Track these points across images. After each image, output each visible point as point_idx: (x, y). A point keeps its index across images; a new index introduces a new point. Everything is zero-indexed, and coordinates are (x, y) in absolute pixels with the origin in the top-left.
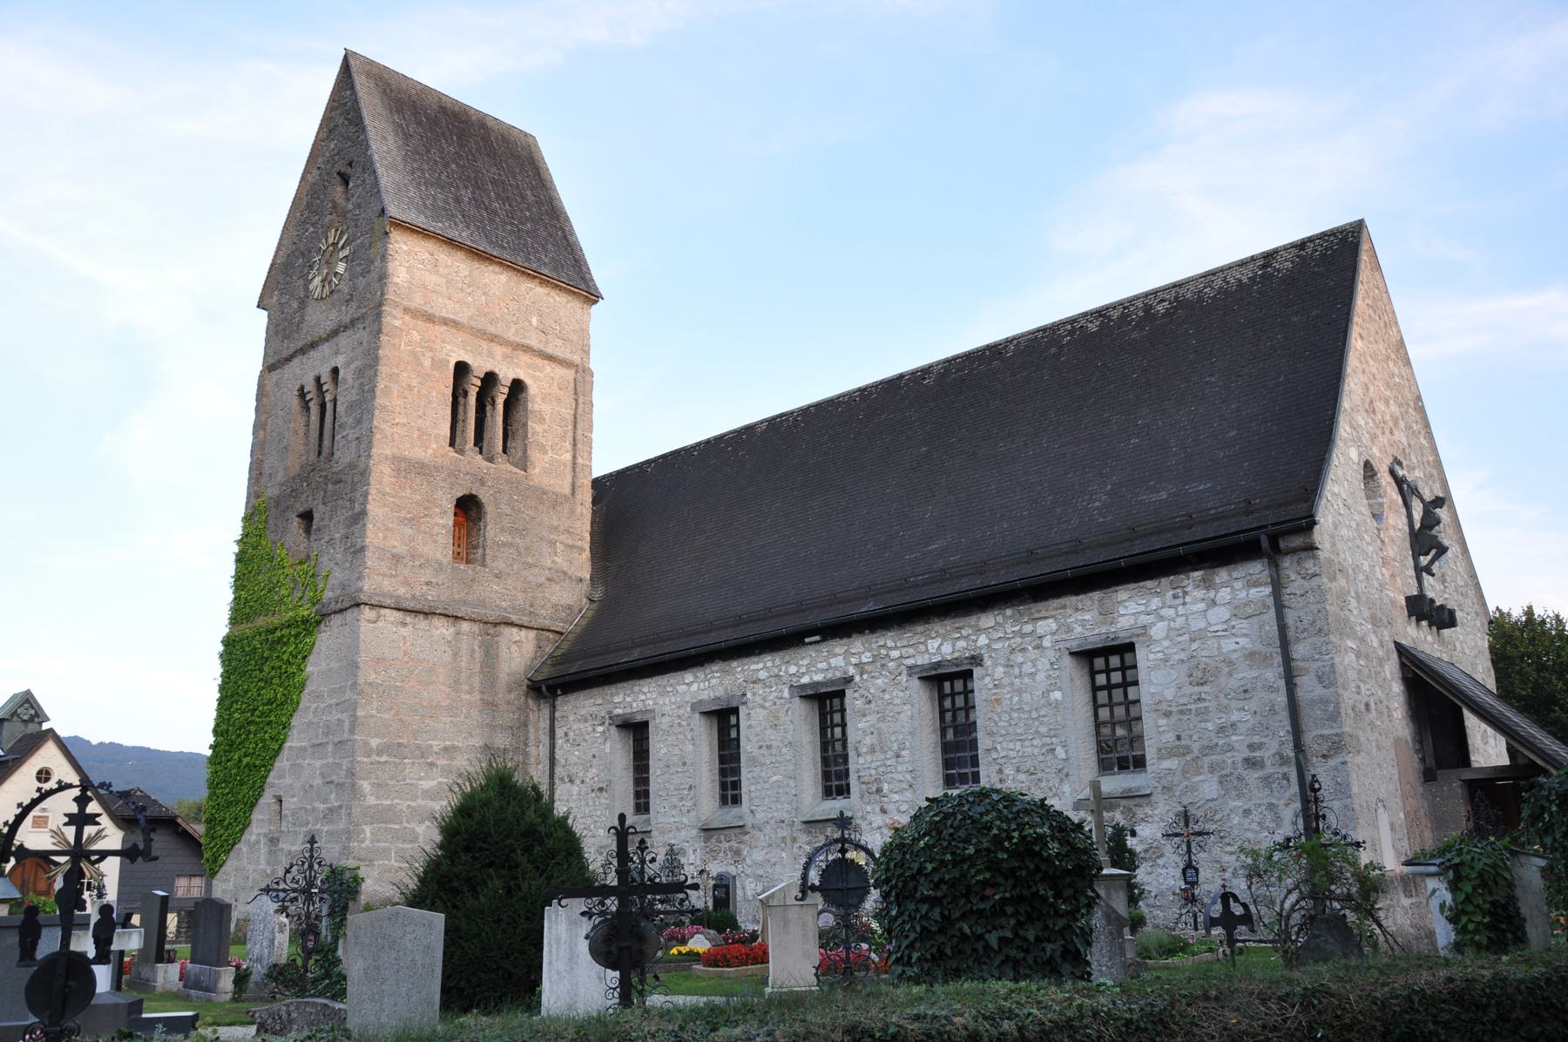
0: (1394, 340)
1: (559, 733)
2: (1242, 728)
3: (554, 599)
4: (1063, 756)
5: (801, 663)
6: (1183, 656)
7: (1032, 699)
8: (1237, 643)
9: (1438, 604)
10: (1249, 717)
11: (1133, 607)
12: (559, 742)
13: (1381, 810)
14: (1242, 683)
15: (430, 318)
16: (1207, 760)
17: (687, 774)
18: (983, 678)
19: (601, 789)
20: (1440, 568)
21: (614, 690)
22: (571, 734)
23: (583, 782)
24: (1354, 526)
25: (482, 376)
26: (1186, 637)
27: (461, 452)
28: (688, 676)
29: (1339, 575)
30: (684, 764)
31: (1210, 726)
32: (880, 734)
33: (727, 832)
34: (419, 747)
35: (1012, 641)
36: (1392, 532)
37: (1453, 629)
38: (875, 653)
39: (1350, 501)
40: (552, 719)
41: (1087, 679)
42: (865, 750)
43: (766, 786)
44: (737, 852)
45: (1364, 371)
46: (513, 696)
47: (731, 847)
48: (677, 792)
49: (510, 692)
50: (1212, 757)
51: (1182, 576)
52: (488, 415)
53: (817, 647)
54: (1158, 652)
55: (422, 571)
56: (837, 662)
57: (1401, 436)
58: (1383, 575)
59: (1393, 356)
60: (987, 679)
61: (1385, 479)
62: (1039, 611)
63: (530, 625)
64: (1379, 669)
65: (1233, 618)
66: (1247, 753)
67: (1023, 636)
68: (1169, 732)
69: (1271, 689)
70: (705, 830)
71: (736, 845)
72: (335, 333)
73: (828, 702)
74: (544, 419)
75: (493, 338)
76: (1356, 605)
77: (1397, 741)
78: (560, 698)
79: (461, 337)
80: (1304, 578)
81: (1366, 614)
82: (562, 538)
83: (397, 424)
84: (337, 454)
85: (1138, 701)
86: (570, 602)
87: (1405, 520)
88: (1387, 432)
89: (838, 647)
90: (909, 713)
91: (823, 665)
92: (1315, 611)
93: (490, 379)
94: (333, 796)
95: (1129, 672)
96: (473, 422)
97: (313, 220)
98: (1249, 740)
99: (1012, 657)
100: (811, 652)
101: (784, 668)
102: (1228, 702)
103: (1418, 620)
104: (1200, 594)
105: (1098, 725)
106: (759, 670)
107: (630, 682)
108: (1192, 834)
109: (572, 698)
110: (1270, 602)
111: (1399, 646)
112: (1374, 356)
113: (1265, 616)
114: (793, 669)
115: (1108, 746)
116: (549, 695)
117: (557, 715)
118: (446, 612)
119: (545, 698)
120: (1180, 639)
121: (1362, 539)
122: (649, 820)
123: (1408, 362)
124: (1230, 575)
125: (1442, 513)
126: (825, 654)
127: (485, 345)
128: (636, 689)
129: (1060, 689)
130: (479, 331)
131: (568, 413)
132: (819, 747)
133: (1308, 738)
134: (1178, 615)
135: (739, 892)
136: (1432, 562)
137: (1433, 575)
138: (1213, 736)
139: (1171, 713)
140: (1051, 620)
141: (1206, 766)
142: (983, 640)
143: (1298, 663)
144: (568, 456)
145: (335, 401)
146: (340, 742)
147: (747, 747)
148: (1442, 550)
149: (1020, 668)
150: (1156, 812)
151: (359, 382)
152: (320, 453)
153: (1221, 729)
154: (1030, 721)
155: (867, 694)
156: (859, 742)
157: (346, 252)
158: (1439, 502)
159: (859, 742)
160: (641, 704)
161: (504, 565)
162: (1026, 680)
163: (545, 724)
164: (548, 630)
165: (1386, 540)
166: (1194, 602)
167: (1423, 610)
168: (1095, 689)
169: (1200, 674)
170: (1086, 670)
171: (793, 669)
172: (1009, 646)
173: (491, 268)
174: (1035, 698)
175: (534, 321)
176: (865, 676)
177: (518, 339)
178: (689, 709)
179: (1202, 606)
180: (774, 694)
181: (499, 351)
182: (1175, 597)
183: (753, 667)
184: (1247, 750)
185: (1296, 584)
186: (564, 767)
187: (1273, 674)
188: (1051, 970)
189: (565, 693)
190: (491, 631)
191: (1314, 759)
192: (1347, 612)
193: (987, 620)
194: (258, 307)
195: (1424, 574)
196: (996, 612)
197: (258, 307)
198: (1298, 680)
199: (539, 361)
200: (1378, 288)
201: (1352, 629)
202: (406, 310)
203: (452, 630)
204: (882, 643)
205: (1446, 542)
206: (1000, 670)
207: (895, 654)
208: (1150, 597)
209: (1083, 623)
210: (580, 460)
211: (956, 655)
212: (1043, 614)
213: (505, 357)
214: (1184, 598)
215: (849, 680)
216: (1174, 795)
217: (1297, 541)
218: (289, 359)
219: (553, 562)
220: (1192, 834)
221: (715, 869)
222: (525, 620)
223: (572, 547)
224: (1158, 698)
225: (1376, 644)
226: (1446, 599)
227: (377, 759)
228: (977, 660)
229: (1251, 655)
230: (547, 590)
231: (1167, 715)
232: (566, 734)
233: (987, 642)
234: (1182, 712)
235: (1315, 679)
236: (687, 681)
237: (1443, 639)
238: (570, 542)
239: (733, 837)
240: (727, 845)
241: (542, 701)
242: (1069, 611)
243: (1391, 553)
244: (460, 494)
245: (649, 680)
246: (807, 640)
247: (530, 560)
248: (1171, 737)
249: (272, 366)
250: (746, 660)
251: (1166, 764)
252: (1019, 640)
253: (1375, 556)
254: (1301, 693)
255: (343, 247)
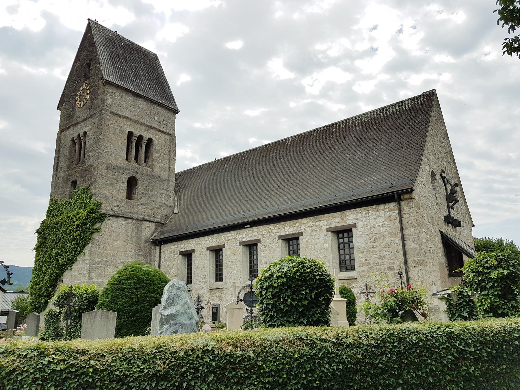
0: (444, 131)
1: (162, 257)
2: (388, 257)
3: (162, 212)
4: (328, 265)
5: (243, 234)
6: (368, 233)
7: (318, 247)
8: (386, 229)
9: (455, 219)
10: (389, 253)
11: (352, 217)
12: (162, 260)
13: (434, 286)
14: (387, 242)
15: (119, 116)
16: (375, 267)
17: (205, 271)
18: (302, 240)
19: (175, 276)
20: (456, 207)
21: (181, 243)
22: (166, 257)
23: (170, 273)
24: (427, 192)
25: (138, 136)
26: (369, 227)
27: (130, 162)
28: (206, 238)
29: (421, 208)
30: (204, 267)
31: (376, 256)
32: (268, 258)
33: (218, 290)
34: (113, 262)
35: (312, 227)
36: (440, 195)
37: (460, 227)
38: (268, 231)
39: (426, 184)
40: (160, 252)
41: (336, 240)
42: (263, 263)
43: (231, 275)
44: (221, 297)
45: (432, 141)
46: (146, 244)
47: (219, 295)
48: (201, 277)
49: (145, 243)
50: (377, 267)
51: (368, 207)
52: (140, 150)
53: (249, 229)
54: (360, 232)
55: (115, 202)
56: (255, 234)
57: (444, 163)
58: (436, 208)
59: (443, 137)
60: (304, 240)
61: (438, 177)
62: (321, 218)
63: (153, 221)
64: (434, 239)
65: (385, 221)
66: (389, 265)
67: (316, 226)
68: (363, 258)
69: (397, 245)
70: (210, 289)
71: (220, 294)
72: (85, 120)
73: (252, 247)
74: (159, 152)
75: (141, 124)
76: (427, 218)
77: (440, 264)
78: (163, 245)
79: (130, 123)
80: (409, 208)
81: (430, 221)
82: (165, 192)
83: (107, 151)
84: (86, 161)
85: (353, 248)
86: (167, 213)
87: (445, 191)
88: (440, 161)
89: (256, 229)
90: (278, 251)
91: (251, 235)
92: (412, 219)
93: (140, 138)
94: (81, 278)
95: (350, 238)
96: (134, 152)
97: (77, 80)
98: (390, 261)
99: (312, 233)
100: (247, 230)
101: (237, 236)
102: (383, 248)
103: (448, 224)
104: (374, 213)
105: (340, 255)
106: (229, 237)
107: (186, 240)
108: (369, 293)
109: (166, 245)
110: (398, 216)
111: (441, 232)
112: (437, 136)
113: (395, 220)
114: (240, 236)
115: (343, 262)
116: (159, 244)
117: (161, 251)
118: (124, 216)
119: (157, 245)
120: (368, 227)
121: (430, 196)
122: (191, 286)
123: (448, 139)
124: (384, 207)
125: (458, 189)
126: (251, 231)
127: (139, 126)
128: (188, 242)
129: (327, 243)
130: (137, 121)
131: (167, 151)
132: (249, 262)
133: (409, 261)
134: (367, 220)
135: (221, 310)
136: (453, 205)
137: (454, 209)
138: (378, 260)
139: (364, 252)
140: (325, 221)
141: (375, 269)
142: (303, 227)
143: (406, 236)
144: (167, 165)
145: (85, 143)
146: (84, 260)
147: (224, 262)
148: (457, 201)
149: (315, 236)
150: (358, 284)
151: (94, 137)
152: (80, 161)
153: (380, 258)
154: (317, 254)
155: (265, 244)
156: (262, 260)
157: (89, 91)
158: (456, 185)
159: (262, 260)
160: (190, 247)
161: (144, 201)
162: (316, 240)
163: (157, 254)
164: (159, 223)
165: (438, 197)
166: (372, 215)
167: (449, 220)
168: (339, 244)
169: (373, 239)
170: (336, 238)
171: (240, 236)
172: (311, 229)
173: (141, 99)
174: (319, 246)
175: (156, 118)
176: (264, 239)
177: (150, 125)
178: (206, 249)
179: (375, 217)
180: (234, 245)
181: (143, 128)
182: (366, 214)
183: (227, 235)
184: (389, 264)
185: (406, 210)
186: (163, 268)
187: (398, 239)
188: (316, 323)
189: (164, 244)
190: (139, 223)
191: (411, 268)
192: (423, 220)
193: (304, 221)
194: (57, 109)
195: (451, 209)
196: (307, 218)
197: (57, 109)
198: (405, 242)
199: (157, 132)
200: (439, 114)
201: (425, 225)
202: (111, 113)
203: (126, 222)
204: (270, 228)
205: (458, 199)
206: (308, 237)
207: (274, 231)
208: (357, 214)
209: (335, 222)
210: (171, 167)
211: (294, 232)
212: (323, 219)
213: (146, 130)
214: (369, 214)
215: (259, 240)
216: (364, 279)
217: (407, 196)
218: (69, 128)
219: (161, 200)
220: (369, 293)
221: (213, 302)
222: (151, 219)
223: (168, 195)
224: (359, 247)
225: (433, 231)
226: (458, 217)
227: (98, 265)
228: (301, 234)
229: (391, 233)
230: (159, 209)
231: (363, 252)
232: (164, 257)
233: (304, 228)
234: (367, 251)
235: (412, 241)
236: (205, 240)
237: (457, 231)
238: (167, 193)
239: (220, 292)
240: (217, 294)
241: (156, 246)
242: (331, 218)
243: (439, 202)
244: (129, 176)
245: (193, 240)
246: (245, 227)
247: (153, 199)
248: (364, 259)
249: (63, 129)
250: (225, 233)
251: (362, 268)
252: (315, 227)
253: (434, 202)
254: (407, 246)
255: (88, 90)
